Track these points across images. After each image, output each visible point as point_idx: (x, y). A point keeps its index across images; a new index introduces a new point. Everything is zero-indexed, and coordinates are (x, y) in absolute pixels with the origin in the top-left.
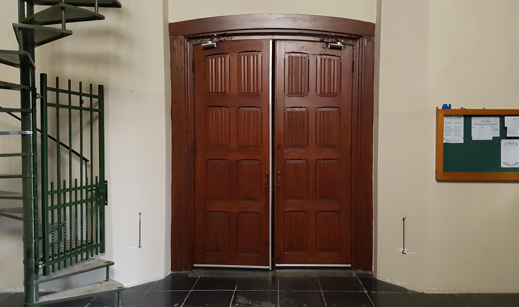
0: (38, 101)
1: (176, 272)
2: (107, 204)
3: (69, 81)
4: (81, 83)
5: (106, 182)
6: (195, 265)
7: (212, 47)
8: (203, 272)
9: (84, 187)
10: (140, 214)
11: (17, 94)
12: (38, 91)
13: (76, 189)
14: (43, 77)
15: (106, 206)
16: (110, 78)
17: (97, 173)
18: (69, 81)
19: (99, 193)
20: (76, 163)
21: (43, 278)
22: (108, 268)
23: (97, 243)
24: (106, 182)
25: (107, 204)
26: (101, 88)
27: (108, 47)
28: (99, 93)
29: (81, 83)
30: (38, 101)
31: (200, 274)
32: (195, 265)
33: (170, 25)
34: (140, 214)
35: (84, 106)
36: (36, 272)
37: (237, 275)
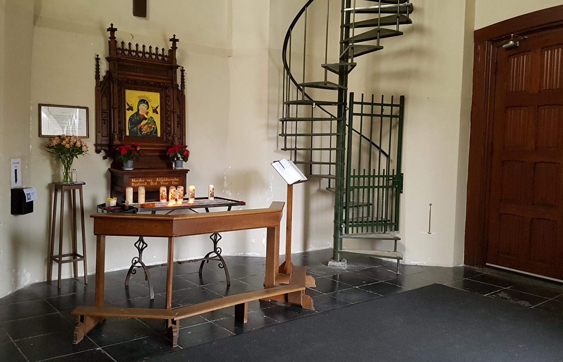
0: (348, 112)
1: (468, 266)
2: (402, 192)
3: (383, 96)
4: (392, 96)
5: (403, 174)
6: (487, 264)
7: (513, 47)
8: (492, 271)
9: (385, 176)
10: (431, 205)
11: (336, 107)
12: (348, 106)
13: (374, 176)
14: (352, 94)
15: (401, 194)
16: (412, 89)
17: (393, 166)
18: (383, 96)
19: (396, 183)
20: (384, 159)
21: (346, 235)
22: (396, 241)
23: (393, 223)
24: (403, 174)
25: (402, 192)
26: (402, 98)
27: (410, 63)
28: (402, 102)
29: (392, 96)
30: (348, 112)
31: (486, 272)
32: (487, 264)
33: (476, 32)
34: (431, 205)
35: (293, 107)
36: (341, 231)
37: (524, 280)
